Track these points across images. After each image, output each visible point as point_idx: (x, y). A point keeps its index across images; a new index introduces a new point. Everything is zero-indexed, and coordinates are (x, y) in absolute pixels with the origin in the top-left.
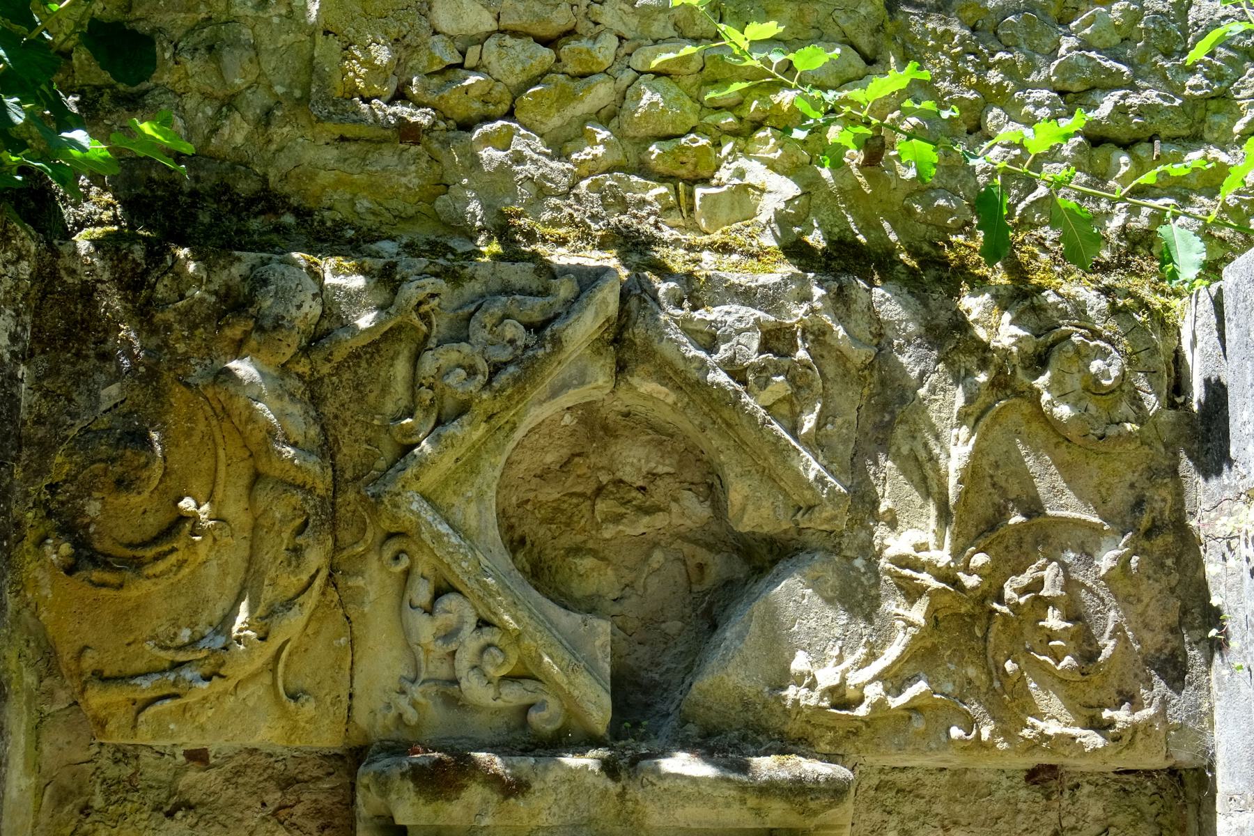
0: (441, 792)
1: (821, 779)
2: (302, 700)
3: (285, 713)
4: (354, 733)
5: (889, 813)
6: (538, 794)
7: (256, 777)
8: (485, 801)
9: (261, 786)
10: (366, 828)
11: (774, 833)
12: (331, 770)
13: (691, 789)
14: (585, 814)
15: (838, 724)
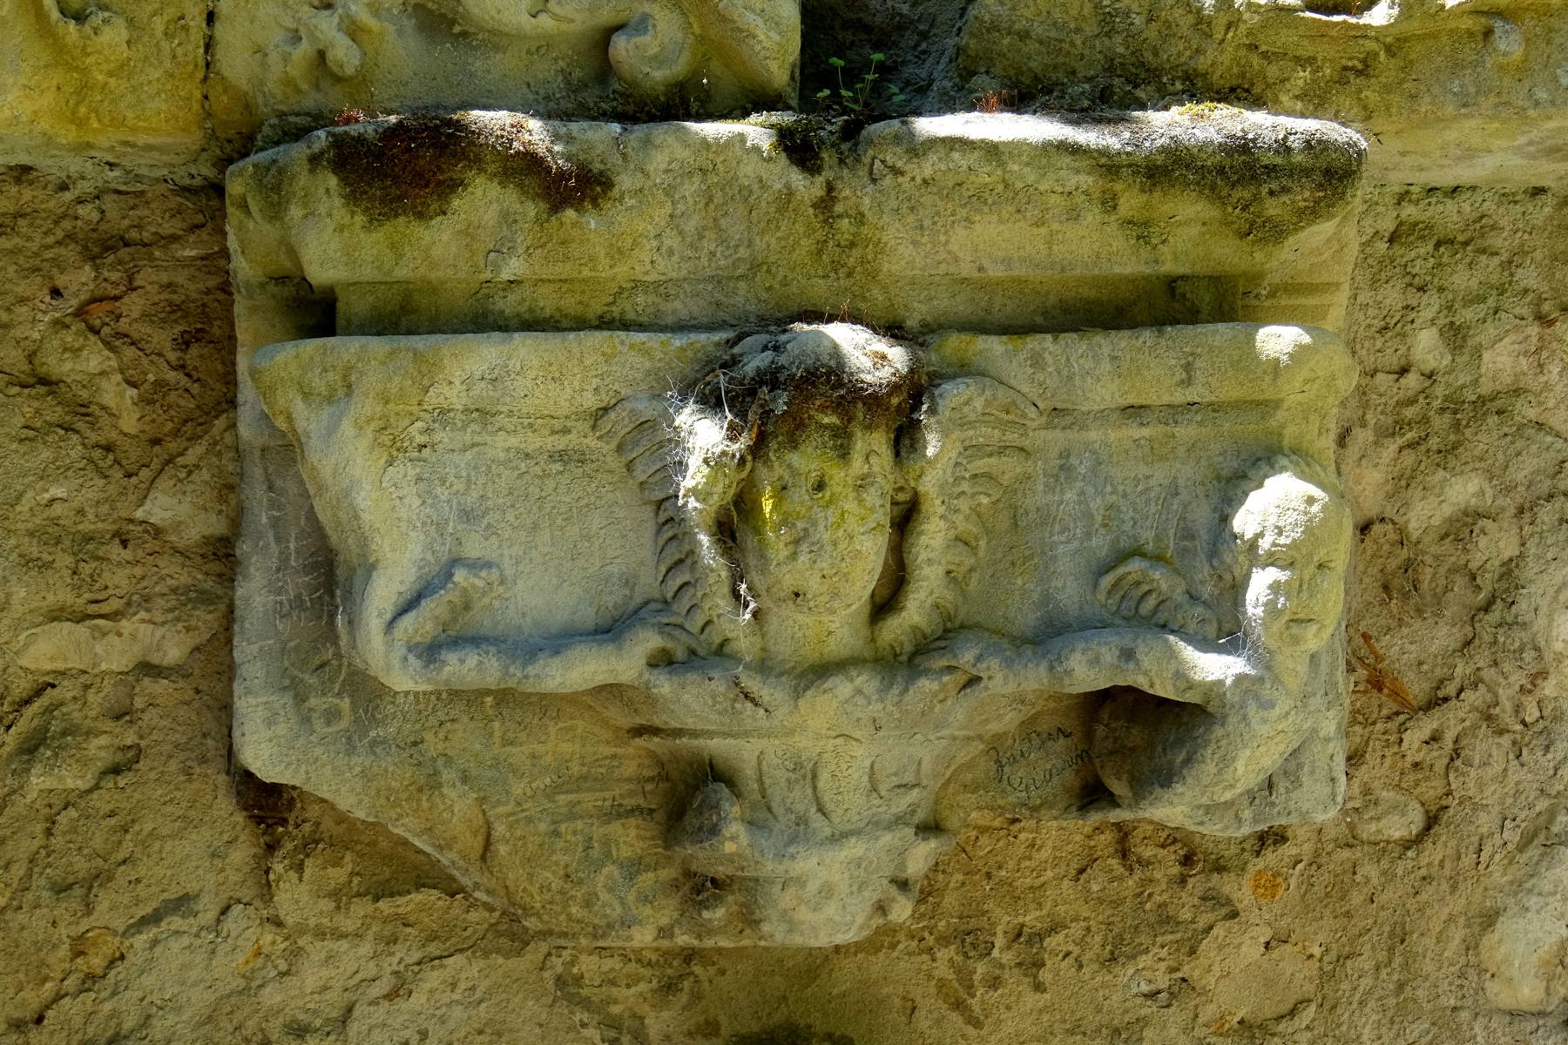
0: (400, 198)
1: (1295, 143)
2: (97, 19)
3: (61, 54)
4: (221, 101)
5: (1422, 289)
6: (630, 202)
7: (38, 237)
8: (508, 219)
9: (49, 255)
10: (253, 310)
11: (1182, 287)
12: (200, 218)
13: (986, 175)
14: (743, 252)
15: (1322, 51)
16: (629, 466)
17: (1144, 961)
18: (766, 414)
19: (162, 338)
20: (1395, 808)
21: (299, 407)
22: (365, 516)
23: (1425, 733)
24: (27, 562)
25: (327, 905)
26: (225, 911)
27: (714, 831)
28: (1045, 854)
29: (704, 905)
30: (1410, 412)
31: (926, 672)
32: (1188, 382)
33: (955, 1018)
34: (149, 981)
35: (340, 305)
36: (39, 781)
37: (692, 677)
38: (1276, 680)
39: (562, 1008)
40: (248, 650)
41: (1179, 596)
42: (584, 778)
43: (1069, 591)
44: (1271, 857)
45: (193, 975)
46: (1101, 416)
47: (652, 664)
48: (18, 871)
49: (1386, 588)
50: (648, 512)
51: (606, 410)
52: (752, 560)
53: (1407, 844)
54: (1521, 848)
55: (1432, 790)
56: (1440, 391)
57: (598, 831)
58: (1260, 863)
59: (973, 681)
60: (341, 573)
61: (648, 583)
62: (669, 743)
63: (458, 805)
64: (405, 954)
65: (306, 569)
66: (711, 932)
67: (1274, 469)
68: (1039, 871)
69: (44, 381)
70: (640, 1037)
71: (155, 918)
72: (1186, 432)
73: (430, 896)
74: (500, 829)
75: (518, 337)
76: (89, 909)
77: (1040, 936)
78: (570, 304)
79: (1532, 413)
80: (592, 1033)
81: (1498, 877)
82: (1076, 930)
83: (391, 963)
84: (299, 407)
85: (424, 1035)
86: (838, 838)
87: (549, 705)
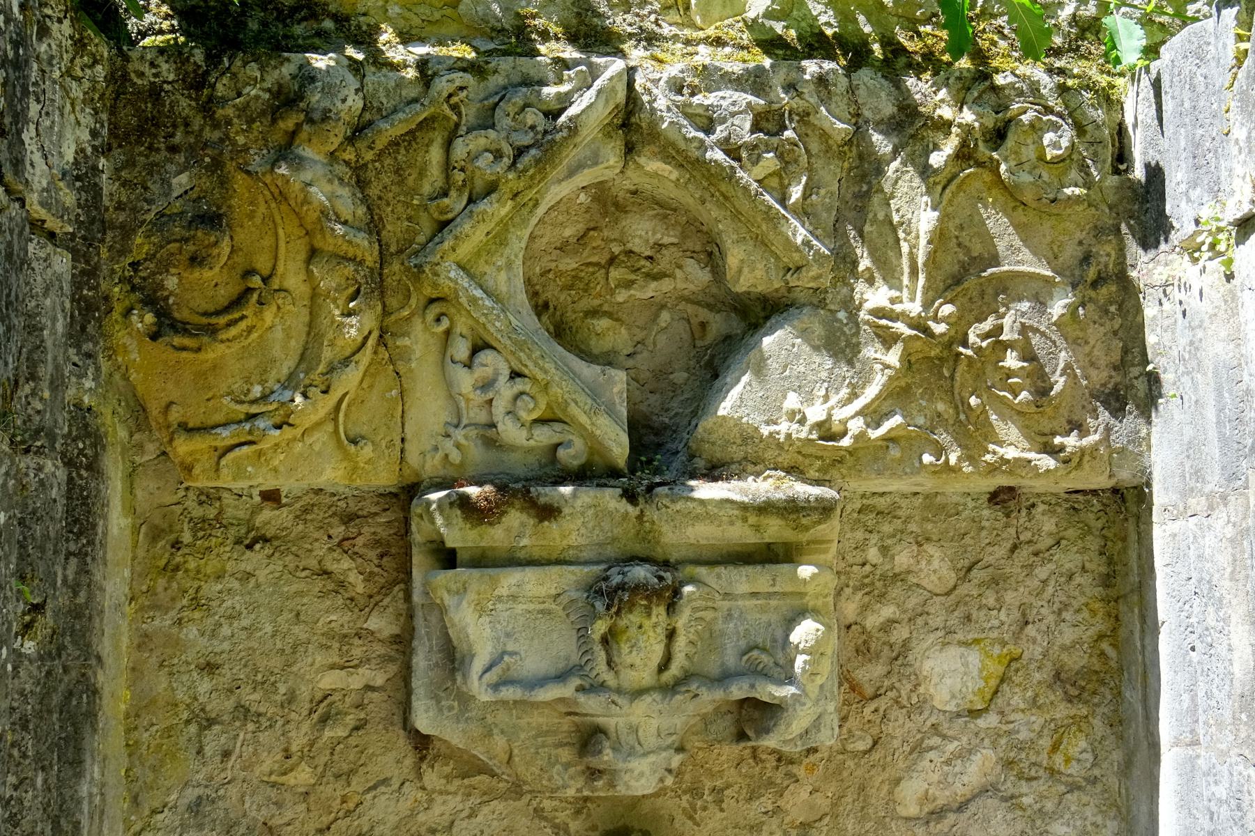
1: (811, 498)
2: (361, 444)
3: (347, 456)
5: (871, 532)
8: (523, 525)
13: (699, 510)
15: (825, 454)
16: (568, 615)
17: (762, 799)
18: (621, 600)
19: (372, 554)
20: (860, 738)
21: (446, 596)
22: (471, 637)
23: (872, 709)
24: (322, 646)
25: (443, 781)
26: (403, 784)
27: (600, 752)
28: (724, 758)
29: (595, 780)
30: (866, 581)
31: (678, 693)
32: (773, 585)
33: (690, 823)
34: (372, 812)
35: (458, 555)
36: (328, 733)
37: (592, 695)
38: (807, 695)
39: (537, 821)
40: (418, 683)
41: (771, 664)
42: (548, 731)
43: (731, 660)
44: (812, 758)
45: (390, 810)
46: (743, 596)
47: (577, 690)
48: (320, 769)
49: (857, 651)
50: (574, 632)
51: (559, 595)
52: (615, 653)
53: (865, 752)
54: (910, 753)
55: (875, 731)
56: (878, 572)
57: (554, 752)
58: (808, 760)
59: (696, 696)
60: (458, 655)
61: (575, 658)
62: (582, 719)
63: (500, 742)
64: (474, 800)
65: (440, 652)
66: (597, 790)
67: (805, 618)
68: (721, 765)
69: (326, 572)
70: (567, 831)
71: (374, 787)
72: (773, 603)
73: (484, 778)
74: (516, 751)
75: (527, 569)
76: (349, 785)
77: (722, 790)
78: (545, 554)
79: (915, 581)
80: (549, 830)
81: (901, 765)
82: (736, 788)
83: (469, 804)
84: (446, 596)
85: (482, 832)
86: (645, 755)
87: (535, 705)
